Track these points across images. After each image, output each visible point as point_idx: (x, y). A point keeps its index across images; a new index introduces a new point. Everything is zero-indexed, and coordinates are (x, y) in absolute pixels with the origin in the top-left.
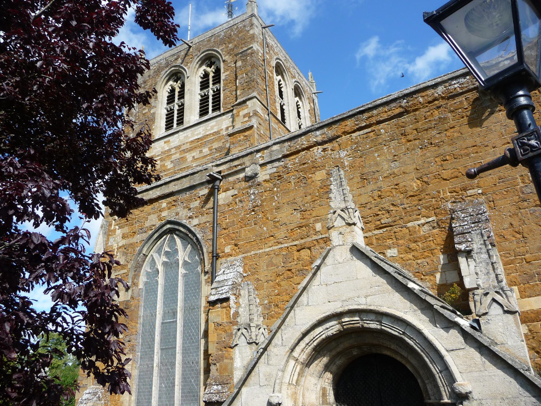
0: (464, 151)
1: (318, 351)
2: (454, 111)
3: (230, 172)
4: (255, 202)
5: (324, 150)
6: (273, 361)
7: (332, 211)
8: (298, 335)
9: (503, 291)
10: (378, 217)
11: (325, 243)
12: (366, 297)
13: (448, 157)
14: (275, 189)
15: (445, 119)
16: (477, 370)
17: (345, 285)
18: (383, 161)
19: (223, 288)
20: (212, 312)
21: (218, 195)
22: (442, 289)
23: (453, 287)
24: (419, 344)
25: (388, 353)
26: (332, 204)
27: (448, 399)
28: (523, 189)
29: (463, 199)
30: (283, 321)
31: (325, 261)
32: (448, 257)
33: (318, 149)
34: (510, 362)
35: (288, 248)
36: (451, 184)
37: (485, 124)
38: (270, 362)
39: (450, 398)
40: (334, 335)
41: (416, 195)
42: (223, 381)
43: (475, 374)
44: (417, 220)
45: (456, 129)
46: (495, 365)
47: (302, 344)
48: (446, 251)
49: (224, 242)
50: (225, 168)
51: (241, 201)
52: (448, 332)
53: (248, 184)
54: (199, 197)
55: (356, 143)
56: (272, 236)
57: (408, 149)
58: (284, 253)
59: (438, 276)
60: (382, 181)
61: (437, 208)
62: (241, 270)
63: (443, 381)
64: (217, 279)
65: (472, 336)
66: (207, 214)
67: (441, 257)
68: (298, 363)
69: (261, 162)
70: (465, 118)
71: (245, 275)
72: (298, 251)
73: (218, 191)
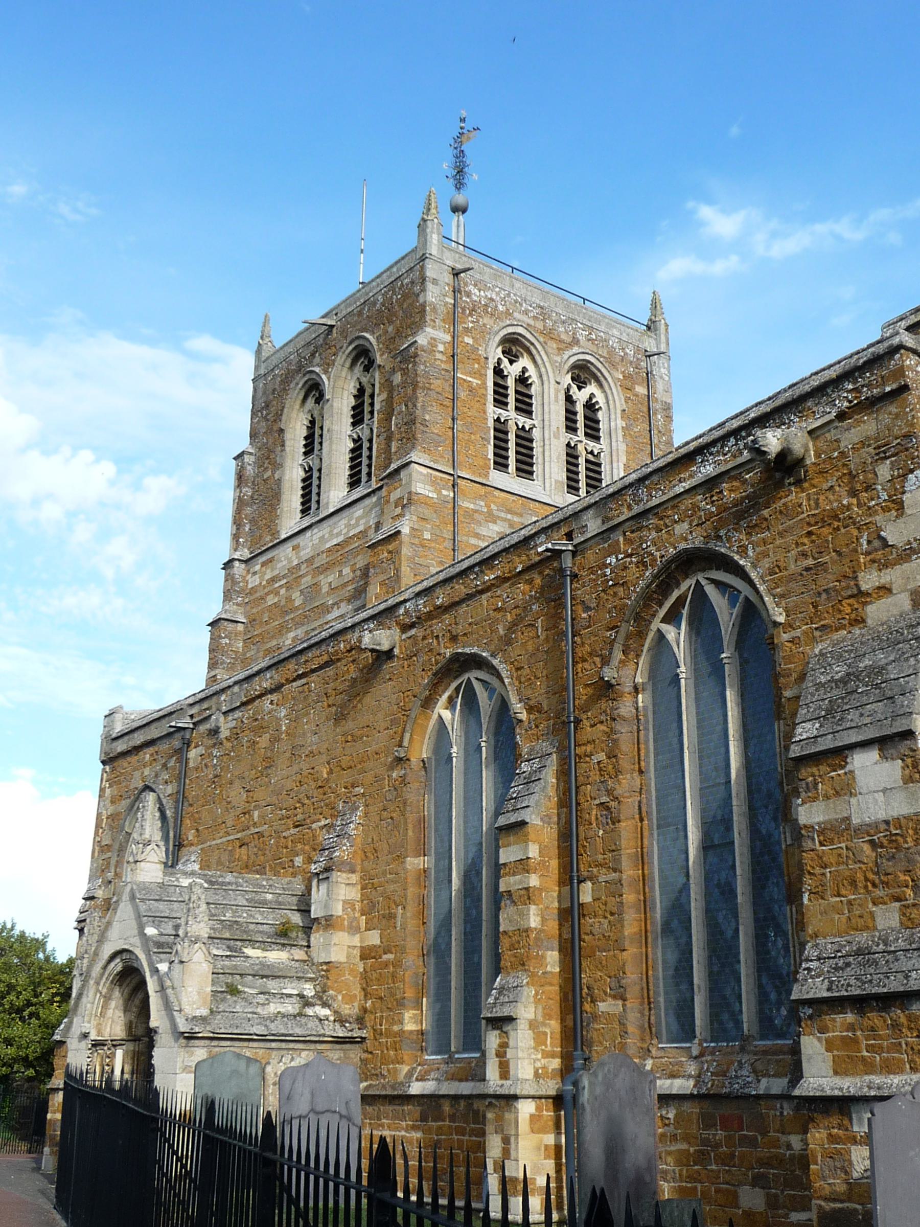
73: (188, 747)
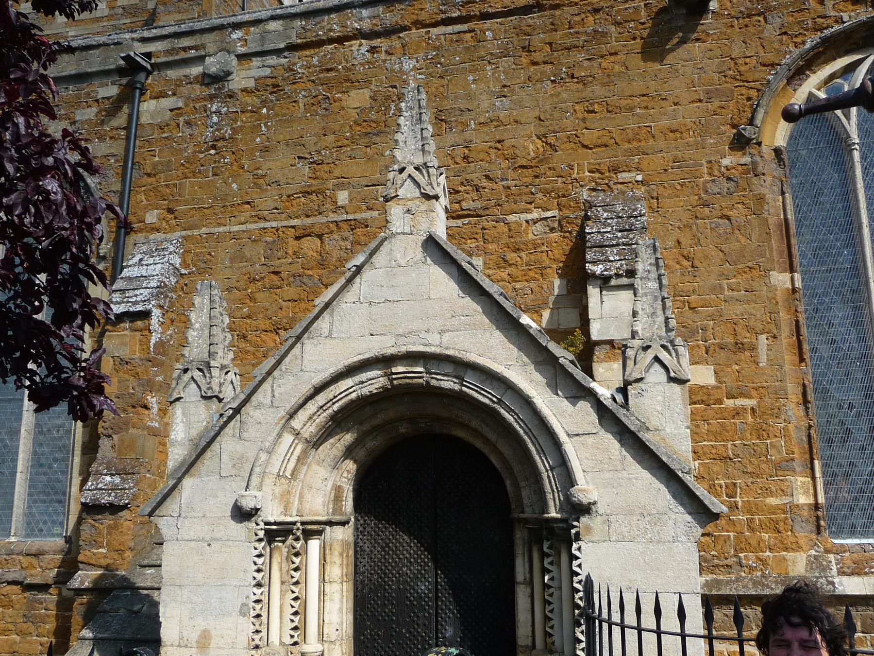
0: (626, 102)
1: (338, 422)
2: (621, 23)
3: (171, 58)
4: (219, 130)
5: (373, 50)
6: (251, 432)
7: (396, 167)
8: (306, 389)
9: (674, 346)
10: (458, 197)
11: (352, 229)
12: (441, 332)
13: (596, 107)
14: (264, 111)
15: (604, 34)
16: (611, 468)
17: (402, 306)
18: (480, 91)
19: (137, 292)
20: (110, 336)
21: (139, 102)
22: (557, 334)
23: (574, 335)
24: (523, 422)
25: (461, 434)
26: (398, 154)
27: (557, 513)
28: (708, 185)
29: (609, 187)
30: (279, 362)
31: (372, 260)
32: (568, 283)
33: (361, 45)
34: (664, 459)
35: (277, 230)
36: (594, 156)
37: (670, 58)
38: (245, 435)
39: (561, 510)
40: (372, 395)
41: (532, 167)
42: (124, 469)
43: (607, 475)
44: (527, 211)
45: (619, 57)
46: (639, 463)
47: (311, 407)
48: (566, 274)
49: (145, 202)
50: (160, 48)
51: (188, 123)
52: (574, 405)
53: (207, 91)
54: (97, 101)
55: (436, 48)
56: (248, 203)
57: (529, 78)
58: (269, 239)
59: (546, 314)
60: (475, 130)
61: (564, 196)
62: (177, 261)
63: (553, 484)
64: (126, 273)
65: (614, 414)
66: (111, 138)
67: (557, 282)
68: (300, 440)
69: (241, 50)
70: (638, 41)
71: (183, 271)
72: (298, 238)
73: (142, 94)
